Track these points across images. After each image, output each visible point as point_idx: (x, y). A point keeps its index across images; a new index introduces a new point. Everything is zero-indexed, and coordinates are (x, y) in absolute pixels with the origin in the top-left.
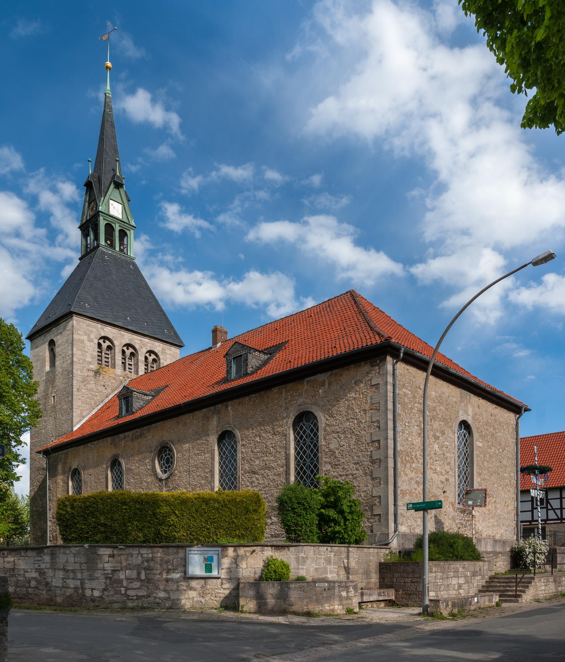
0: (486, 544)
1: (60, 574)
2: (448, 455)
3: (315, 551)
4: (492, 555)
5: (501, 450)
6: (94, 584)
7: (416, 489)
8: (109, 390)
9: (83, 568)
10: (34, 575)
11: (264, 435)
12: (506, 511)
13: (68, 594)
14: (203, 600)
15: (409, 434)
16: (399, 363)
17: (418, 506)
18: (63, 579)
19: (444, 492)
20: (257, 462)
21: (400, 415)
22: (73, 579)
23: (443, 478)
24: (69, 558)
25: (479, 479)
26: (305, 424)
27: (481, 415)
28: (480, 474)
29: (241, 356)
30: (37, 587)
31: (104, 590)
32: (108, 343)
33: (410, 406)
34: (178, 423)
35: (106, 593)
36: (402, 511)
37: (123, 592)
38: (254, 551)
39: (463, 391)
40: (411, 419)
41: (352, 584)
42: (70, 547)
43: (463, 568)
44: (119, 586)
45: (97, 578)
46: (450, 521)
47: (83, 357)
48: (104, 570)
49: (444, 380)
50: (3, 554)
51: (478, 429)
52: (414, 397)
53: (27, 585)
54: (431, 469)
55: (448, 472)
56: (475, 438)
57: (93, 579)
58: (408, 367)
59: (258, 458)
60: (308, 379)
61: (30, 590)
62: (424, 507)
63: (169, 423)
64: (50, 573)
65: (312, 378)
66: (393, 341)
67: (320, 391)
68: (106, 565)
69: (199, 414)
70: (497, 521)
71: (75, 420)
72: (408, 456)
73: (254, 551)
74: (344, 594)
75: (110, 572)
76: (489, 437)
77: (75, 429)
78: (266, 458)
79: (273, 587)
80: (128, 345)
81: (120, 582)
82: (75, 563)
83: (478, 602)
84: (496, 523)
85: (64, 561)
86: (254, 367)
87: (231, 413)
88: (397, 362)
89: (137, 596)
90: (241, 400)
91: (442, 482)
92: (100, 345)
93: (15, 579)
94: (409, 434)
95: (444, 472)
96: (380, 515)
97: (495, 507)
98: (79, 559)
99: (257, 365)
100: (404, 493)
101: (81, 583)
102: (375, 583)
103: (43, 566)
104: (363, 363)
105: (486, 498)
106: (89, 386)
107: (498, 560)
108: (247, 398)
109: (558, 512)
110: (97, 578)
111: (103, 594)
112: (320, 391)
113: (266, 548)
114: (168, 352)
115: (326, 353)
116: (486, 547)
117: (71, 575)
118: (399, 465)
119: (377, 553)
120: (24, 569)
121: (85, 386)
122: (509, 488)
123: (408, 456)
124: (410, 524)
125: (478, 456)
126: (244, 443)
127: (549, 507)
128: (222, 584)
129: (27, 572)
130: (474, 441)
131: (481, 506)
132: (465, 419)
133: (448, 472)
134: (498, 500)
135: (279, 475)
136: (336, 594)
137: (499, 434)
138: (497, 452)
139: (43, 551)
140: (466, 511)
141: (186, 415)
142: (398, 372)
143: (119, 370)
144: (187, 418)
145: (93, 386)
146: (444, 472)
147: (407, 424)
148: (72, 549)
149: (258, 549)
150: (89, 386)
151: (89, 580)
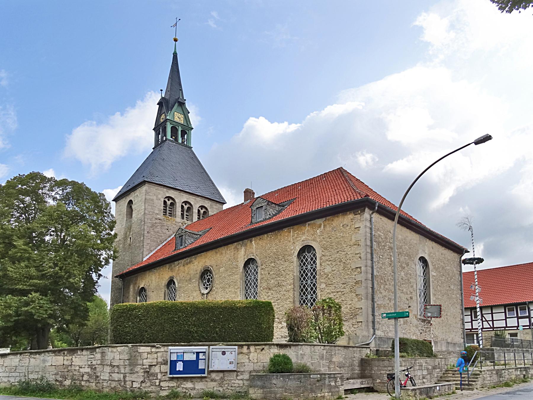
0: (441, 345)
1: (108, 369)
2: (411, 280)
3: (311, 349)
4: (446, 353)
5: (449, 279)
6: (133, 377)
7: (388, 304)
8: (171, 232)
9: (126, 364)
10: (88, 370)
11: (278, 262)
12: (454, 322)
13: (113, 386)
14: (221, 389)
15: (382, 264)
16: (374, 214)
17: (390, 315)
18: (109, 373)
19: (409, 307)
20: (272, 281)
21: (376, 250)
22: (118, 373)
23: (408, 297)
24: (115, 356)
25: (435, 299)
26: (308, 255)
27: (435, 254)
28: (435, 295)
29: (262, 206)
30: (88, 381)
31: (142, 382)
32: (171, 201)
33: (383, 244)
34: (216, 253)
35: (143, 385)
36: (378, 320)
37: (157, 384)
38: (263, 349)
39: (421, 236)
40: (384, 253)
41: (339, 376)
42: (117, 347)
43: (426, 363)
44: (155, 378)
45: (137, 372)
46: (415, 328)
47: (152, 211)
48: (143, 365)
49: (407, 228)
50: (64, 353)
51: (432, 263)
52: (386, 238)
53: (81, 378)
54: (399, 289)
55: (411, 293)
56: (430, 270)
57: (134, 373)
58: (381, 217)
59: (272, 279)
60: (309, 222)
61: (83, 383)
62: (397, 316)
63: (210, 254)
64: (99, 368)
65: (312, 222)
66: (370, 197)
67: (318, 231)
68: (145, 361)
69: (232, 247)
70: (449, 328)
71: (145, 253)
72: (382, 279)
73: (263, 349)
74: (333, 384)
75: (148, 366)
76: (441, 269)
77: (144, 259)
78: (278, 279)
79: (277, 378)
80: (186, 202)
81: (155, 375)
82: (120, 359)
83: (439, 390)
84: (448, 330)
85: (112, 358)
86: (271, 214)
87: (254, 245)
88: (373, 213)
89: (168, 387)
90: (261, 237)
91: (408, 300)
92: (165, 202)
93: (71, 374)
94: (382, 264)
95: (409, 292)
96: (361, 322)
97: (447, 318)
98: (123, 356)
99: (274, 213)
100: (379, 307)
101: (124, 377)
102: (358, 374)
103: (94, 363)
104: (348, 213)
105: (441, 311)
106: (156, 230)
107: (451, 356)
108: (266, 236)
109: (491, 323)
110: (137, 372)
111: (141, 386)
112: (318, 231)
113: (272, 347)
114: (215, 207)
115: (322, 205)
116: (441, 347)
117: (116, 370)
118: (375, 286)
119: (360, 351)
120: (79, 366)
121: (153, 229)
122: (456, 306)
123: (382, 279)
124: (384, 329)
125: (433, 282)
126: (263, 267)
127: (484, 320)
128: (237, 376)
129: (81, 368)
130: (430, 271)
131: (437, 317)
132: (423, 256)
133: (411, 293)
134: (449, 314)
135: (288, 291)
136: (327, 384)
137: (448, 268)
138: (446, 280)
139: (96, 350)
140: (426, 320)
141: (223, 248)
142: (373, 220)
143: (178, 219)
144: (223, 250)
145: (159, 230)
146: (409, 292)
147: (381, 257)
148: (118, 348)
149: (266, 347)
150: (156, 230)
151: (131, 373)
